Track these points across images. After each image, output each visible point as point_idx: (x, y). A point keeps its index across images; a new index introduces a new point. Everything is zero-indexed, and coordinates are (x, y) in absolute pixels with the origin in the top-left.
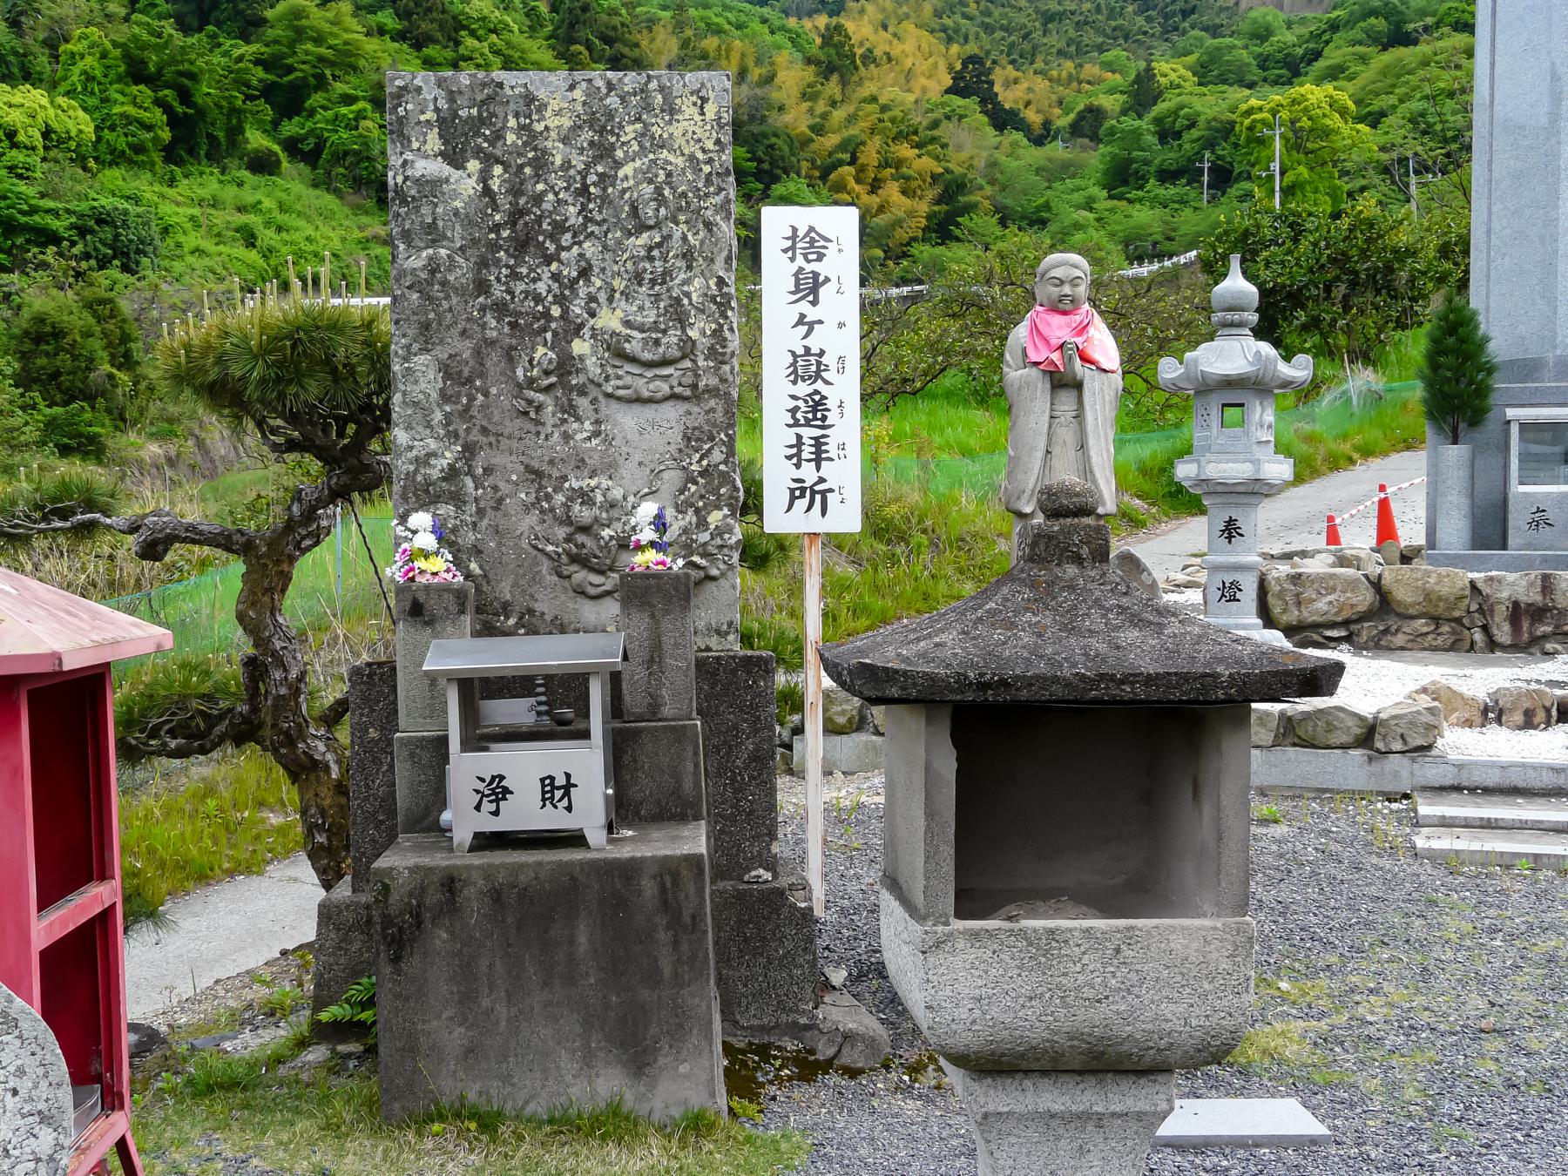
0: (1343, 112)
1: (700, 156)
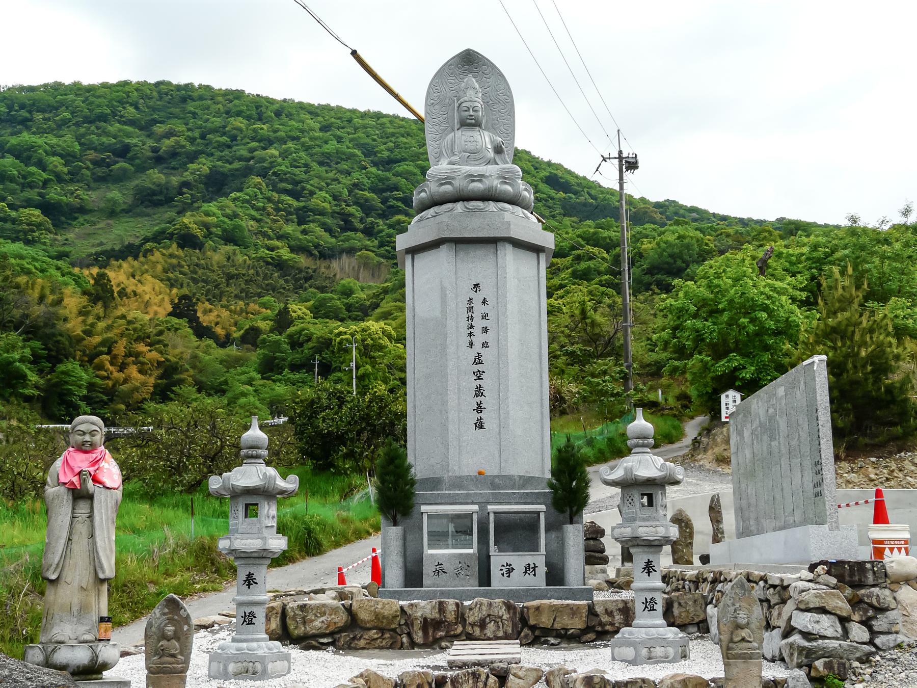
0: (390, 337)
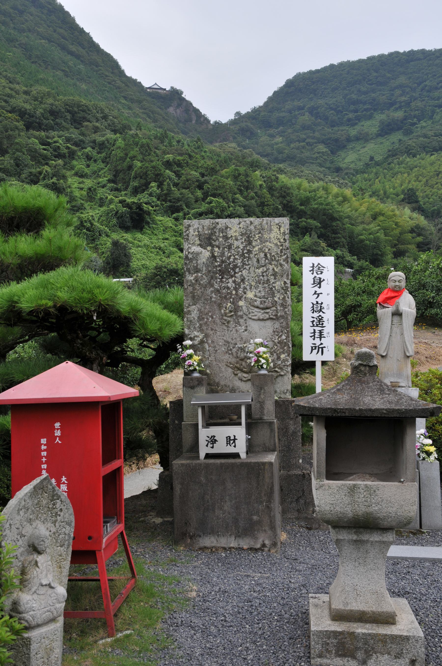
1: (279, 244)
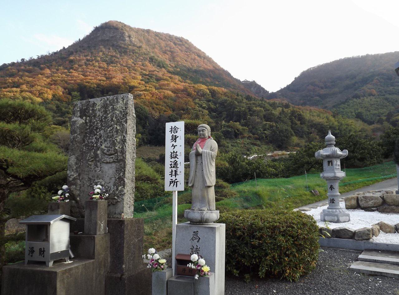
1: (122, 111)
